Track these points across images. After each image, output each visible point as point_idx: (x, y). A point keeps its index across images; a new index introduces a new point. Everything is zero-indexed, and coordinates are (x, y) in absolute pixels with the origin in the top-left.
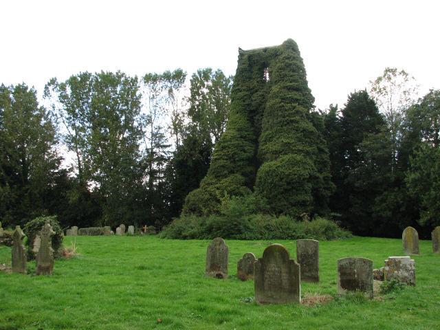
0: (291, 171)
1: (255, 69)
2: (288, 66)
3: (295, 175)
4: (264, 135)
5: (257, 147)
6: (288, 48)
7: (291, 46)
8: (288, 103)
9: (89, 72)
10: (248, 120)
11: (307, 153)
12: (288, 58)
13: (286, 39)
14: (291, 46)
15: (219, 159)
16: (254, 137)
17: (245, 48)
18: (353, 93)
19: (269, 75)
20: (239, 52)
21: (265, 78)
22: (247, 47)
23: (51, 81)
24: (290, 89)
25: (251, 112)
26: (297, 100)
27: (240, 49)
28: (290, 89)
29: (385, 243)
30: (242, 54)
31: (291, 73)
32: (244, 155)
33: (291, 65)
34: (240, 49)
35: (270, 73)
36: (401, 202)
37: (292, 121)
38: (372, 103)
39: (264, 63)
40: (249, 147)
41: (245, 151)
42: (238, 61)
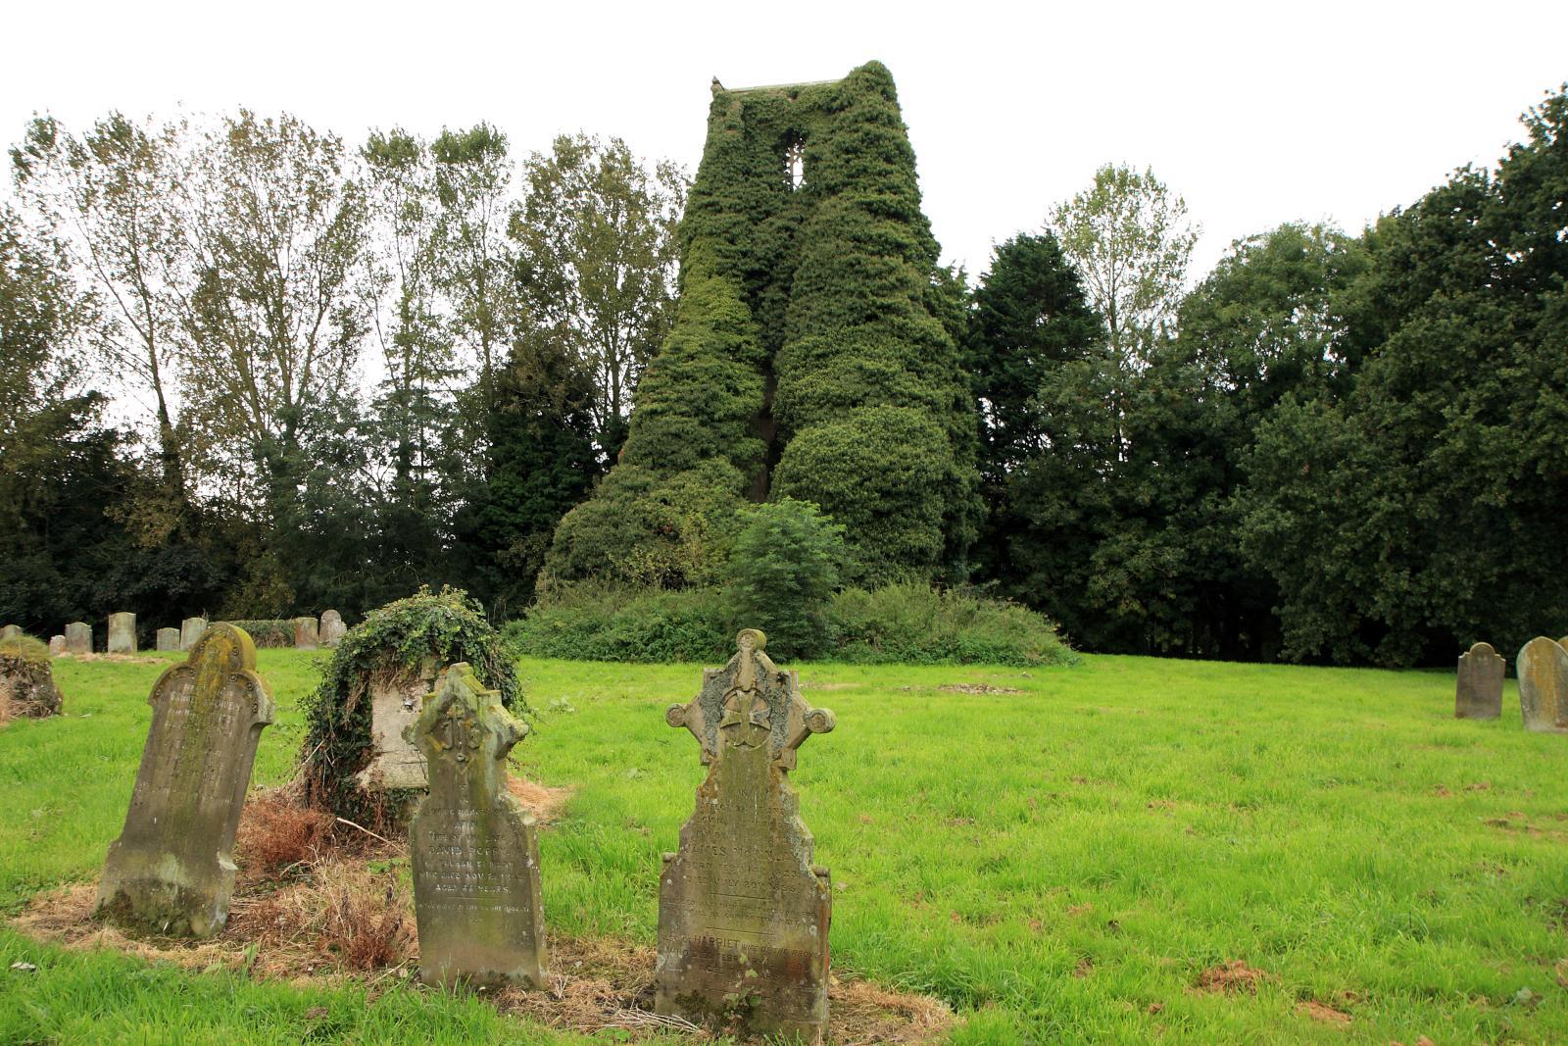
0: (894, 458)
1: (765, 141)
2: (872, 140)
3: (908, 469)
4: (793, 347)
5: (771, 386)
6: (870, 88)
7: (876, 80)
8: (872, 254)
9: (105, 119)
10: (742, 299)
11: (933, 406)
12: (871, 120)
13: (861, 62)
14: (876, 80)
15: (663, 413)
16: (763, 353)
17: (730, 84)
18: (1002, 242)
19: (806, 171)
20: (714, 91)
21: (790, 178)
22: (742, 79)
23: (395, 144)
24: (873, 210)
25: (751, 275)
26: (900, 247)
27: (716, 82)
28: (873, 210)
29: (1209, 677)
30: (722, 101)
31: (882, 165)
32: (737, 404)
33: (878, 138)
34: (716, 82)
35: (812, 161)
36: (1437, 517)
37: (887, 309)
38: (1071, 277)
39: (790, 130)
40: (752, 385)
41: (737, 393)
42: (711, 121)
